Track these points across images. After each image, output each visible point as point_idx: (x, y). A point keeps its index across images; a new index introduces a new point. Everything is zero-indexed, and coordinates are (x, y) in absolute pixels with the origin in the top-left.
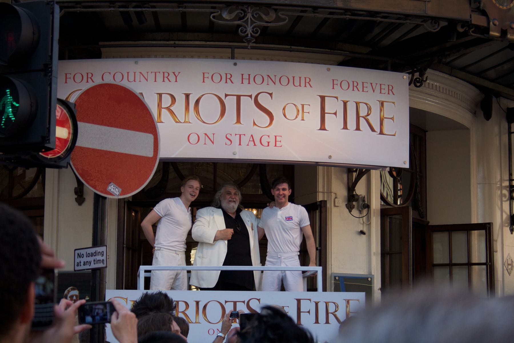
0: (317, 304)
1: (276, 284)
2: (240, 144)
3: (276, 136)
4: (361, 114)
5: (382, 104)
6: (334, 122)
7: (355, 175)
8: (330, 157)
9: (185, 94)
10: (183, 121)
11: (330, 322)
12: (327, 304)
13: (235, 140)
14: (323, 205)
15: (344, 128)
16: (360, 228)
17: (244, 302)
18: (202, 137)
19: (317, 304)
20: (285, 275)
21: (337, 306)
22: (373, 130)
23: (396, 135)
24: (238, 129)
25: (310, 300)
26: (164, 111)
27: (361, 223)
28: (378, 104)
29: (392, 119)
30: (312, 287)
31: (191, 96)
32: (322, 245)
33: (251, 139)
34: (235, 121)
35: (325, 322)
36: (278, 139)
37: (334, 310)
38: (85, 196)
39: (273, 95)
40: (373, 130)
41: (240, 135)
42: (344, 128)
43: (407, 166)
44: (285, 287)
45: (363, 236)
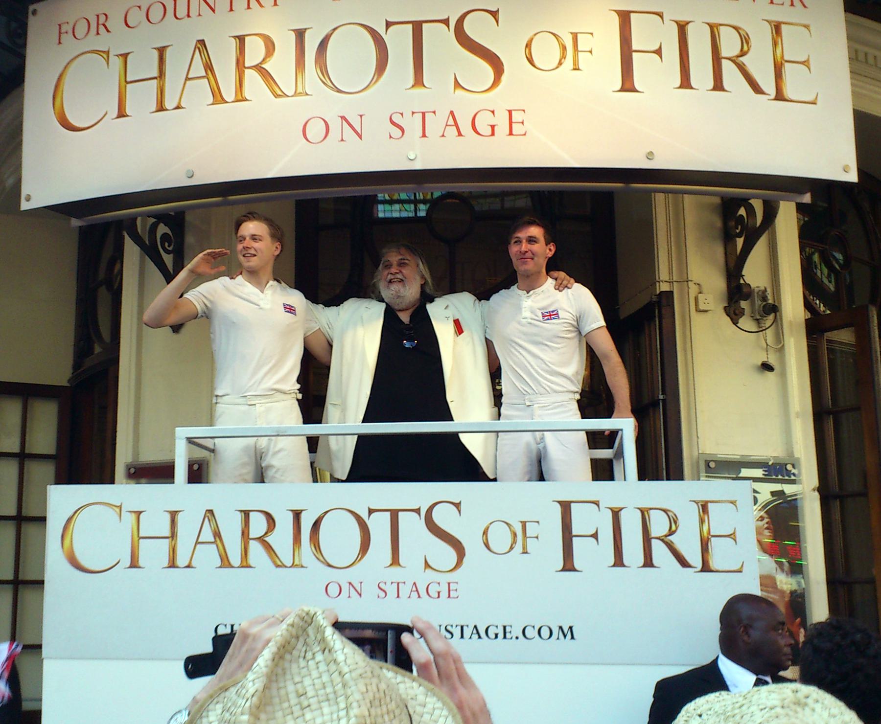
0: (616, 514)
2: (424, 135)
3: (510, 112)
4: (725, 52)
5: (777, 28)
6: (655, 73)
7: (740, 242)
8: (650, 156)
9: (294, 30)
10: (292, 93)
11: (655, 562)
12: (644, 513)
13: (413, 125)
14: (664, 301)
15: (682, 86)
16: (762, 358)
17: (418, 511)
19: (616, 514)
21: (673, 520)
22: (756, 88)
23: (819, 102)
24: (420, 99)
25: (597, 503)
26: (251, 75)
27: (762, 348)
28: (768, 30)
29: (806, 63)
30: (603, 471)
31: (307, 35)
32: (668, 389)
33: (451, 122)
34: (411, 81)
35: (641, 561)
36: (516, 117)
37: (666, 531)
39: (501, 16)
40: (756, 88)
41: (424, 114)
42: (682, 86)
43: (852, 177)
44: (545, 476)
45: (769, 374)
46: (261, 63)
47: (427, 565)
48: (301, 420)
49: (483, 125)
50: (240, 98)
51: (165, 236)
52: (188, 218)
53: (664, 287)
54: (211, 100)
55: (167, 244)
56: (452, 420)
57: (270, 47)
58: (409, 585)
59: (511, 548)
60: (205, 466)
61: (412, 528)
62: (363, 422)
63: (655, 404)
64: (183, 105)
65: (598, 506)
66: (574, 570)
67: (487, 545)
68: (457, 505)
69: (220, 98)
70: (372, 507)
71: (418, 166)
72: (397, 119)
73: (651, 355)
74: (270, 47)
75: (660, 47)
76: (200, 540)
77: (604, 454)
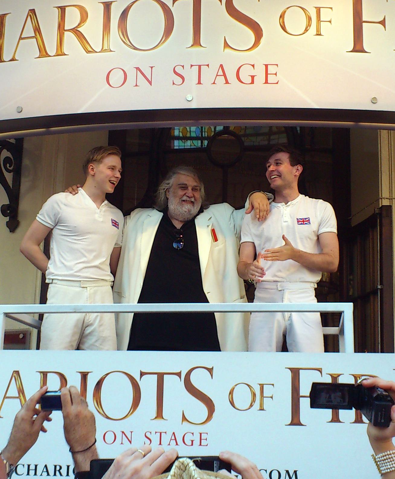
1: (275, 339)
2: (199, 83)
3: (266, 66)
8: (374, 101)
13: (191, 75)
14: (384, 213)
17: (179, 374)
18: (132, 74)
20: (291, 325)
24: (197, 55)
26: (69, 37)
30: (331, 344)
32: (385, 282)
33: (221, 73)
36: (271, 69)
38: (20, 218)
41: (200, 66)
46: (76, 27)
47: (184, 418)
48: (316, 300)
49: (245, 76)
50: (60, 53)
51: (7, 160)
52: (26, 145)
53: (386, 203)
54: (38, 54)
55: (8, 165)
56: (208, 302)
57: (84, 16)
58: (170, 434)
59: (251, 406)
60: (28, 336)
61: (174, 387)
62: (138, 303)
63: (374, 292)
64: (16, 58)
65: (321, 373)
66: (300, 424)
67: (232, 403)
68: (210, 370)
69: (45, 54)
70: (143, 371)
71: (194, 105)
72: (179, 70)
73: (373, 254)
74: (84, 16)
75: (384, 19)
76: (7, 395)
77: (332, 330)
